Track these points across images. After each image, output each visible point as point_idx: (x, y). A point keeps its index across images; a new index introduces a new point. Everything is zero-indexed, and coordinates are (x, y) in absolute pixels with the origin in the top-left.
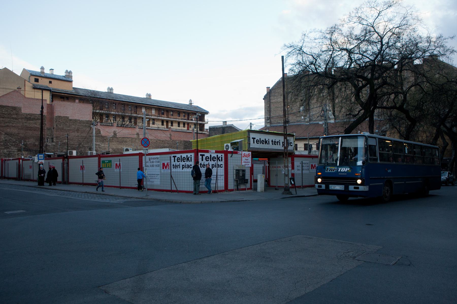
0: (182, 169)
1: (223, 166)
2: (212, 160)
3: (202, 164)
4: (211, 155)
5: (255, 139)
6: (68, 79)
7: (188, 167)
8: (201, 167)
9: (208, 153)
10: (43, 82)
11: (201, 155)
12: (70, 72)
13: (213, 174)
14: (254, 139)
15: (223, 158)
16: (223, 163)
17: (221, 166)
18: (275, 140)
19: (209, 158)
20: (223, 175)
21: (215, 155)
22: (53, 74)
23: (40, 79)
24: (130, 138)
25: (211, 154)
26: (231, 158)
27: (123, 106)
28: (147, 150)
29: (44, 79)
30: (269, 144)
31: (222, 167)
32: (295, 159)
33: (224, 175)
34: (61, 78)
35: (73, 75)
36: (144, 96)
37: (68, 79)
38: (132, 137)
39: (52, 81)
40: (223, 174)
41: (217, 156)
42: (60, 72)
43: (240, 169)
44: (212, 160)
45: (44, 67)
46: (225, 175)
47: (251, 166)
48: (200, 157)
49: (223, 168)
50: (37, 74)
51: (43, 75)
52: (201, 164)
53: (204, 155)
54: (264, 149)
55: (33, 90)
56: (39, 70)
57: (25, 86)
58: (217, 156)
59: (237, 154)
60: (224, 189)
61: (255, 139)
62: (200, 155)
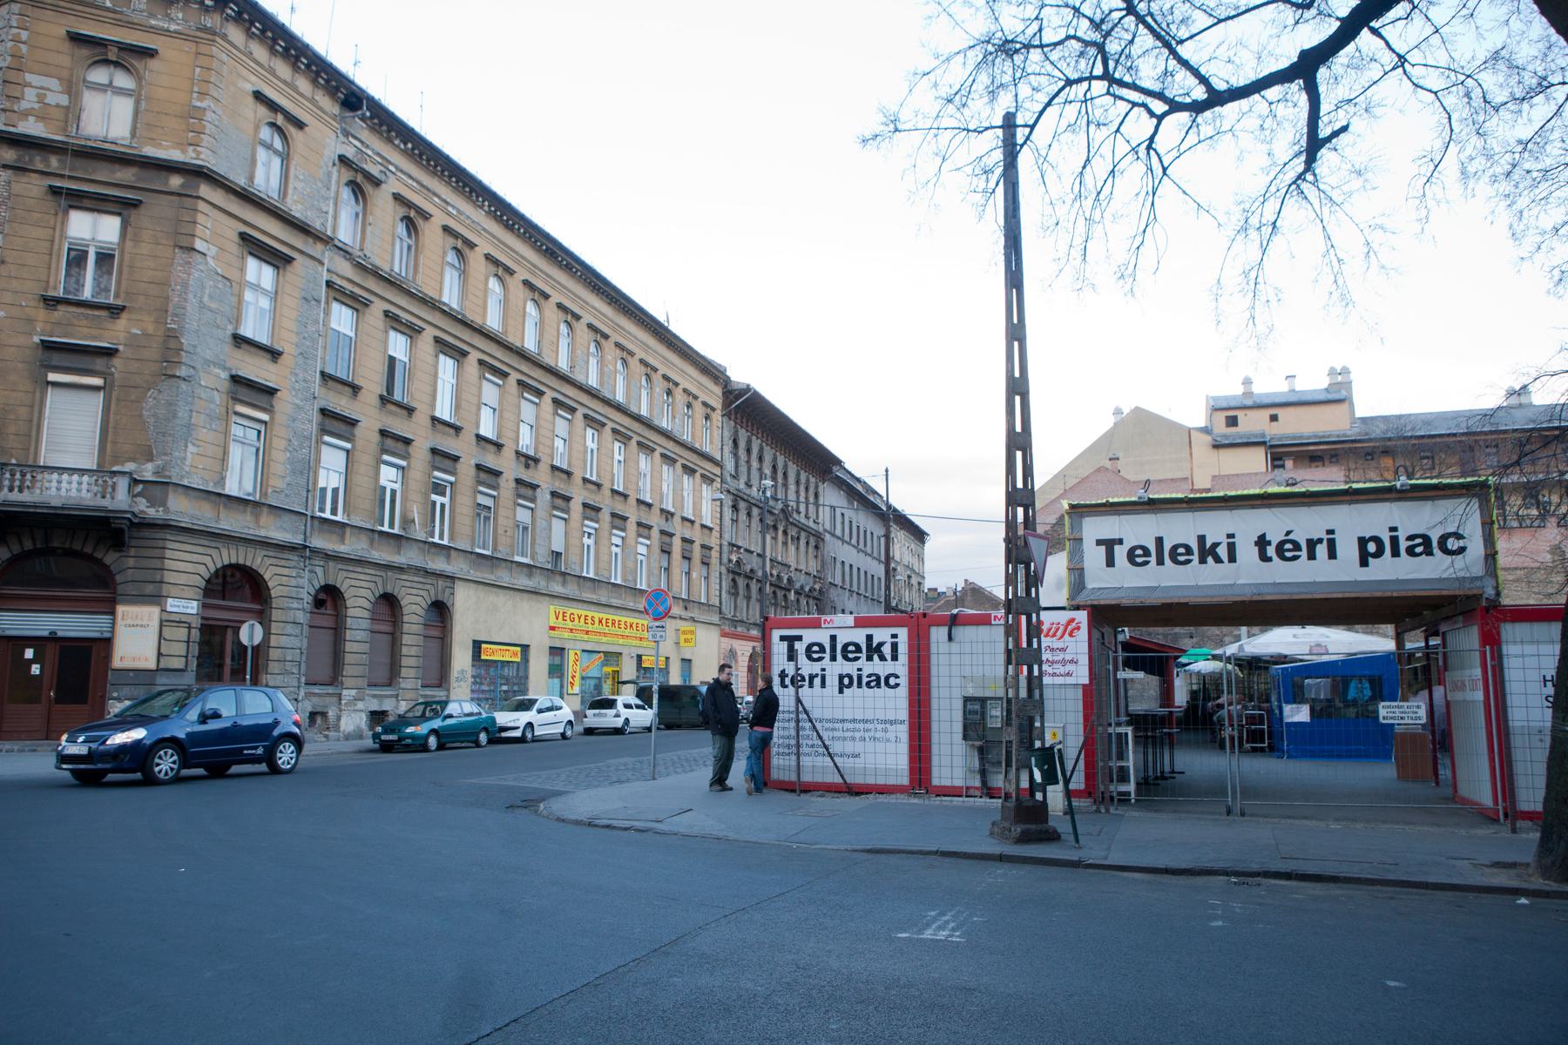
0: (841, 691)
1: (904, 681)
2: (839, 657)
3: (791, 671)
4: (833, 638)
5: (1117, 548)
6: (1337, 396)
7: (873, 684)
8: (784, 686)
9: (820, 627)
10: (1254, 424)
11: (783, 638)
12: (1345, 371)
13: (781, 709)
14: (1110, 545)
15: (903, 649)
16: (901, 667)
17: (892, 681)
18: (1288, 533)
19: (822, 650)
20: (902, 722)
21: (859, 636)
22: (1294, 391)
23: (1240, 414)
24: (1516, 569)
25: (833, 632)
26: (953, 645)
27: (1494, 450)
28: (663, 627)
29: (1253, 414)
30: (1232, 559)
31: (897, 685)
32: (1509, 631)
33: (907, 723)
34: (1322, 397)
35: (1353, 377)
36: (1491, 400)
37: (1337, 396)
38: (1526, 565)
39: (1279, 412)
40: (903, 714)
41: (869, 638)
42: (1313, 381)
43: (988, 694)
44: (839, 657)
45: (1348, 366)
46: (910, 723)
47: (1086, 681)
48: (779, 649)
49: (903, 691)
50: (1233, 404)
51: (1249, 402)
52: (783, 675)
53: (800, 638)
54: (1296, 590)
55: (1216, 451)
56: (1239, 390)
57: (1191, 447)
58: (869, 638)
59: (990, 624)
60: (905, 781)
61: (1117, 548)
62: (867, 636)
